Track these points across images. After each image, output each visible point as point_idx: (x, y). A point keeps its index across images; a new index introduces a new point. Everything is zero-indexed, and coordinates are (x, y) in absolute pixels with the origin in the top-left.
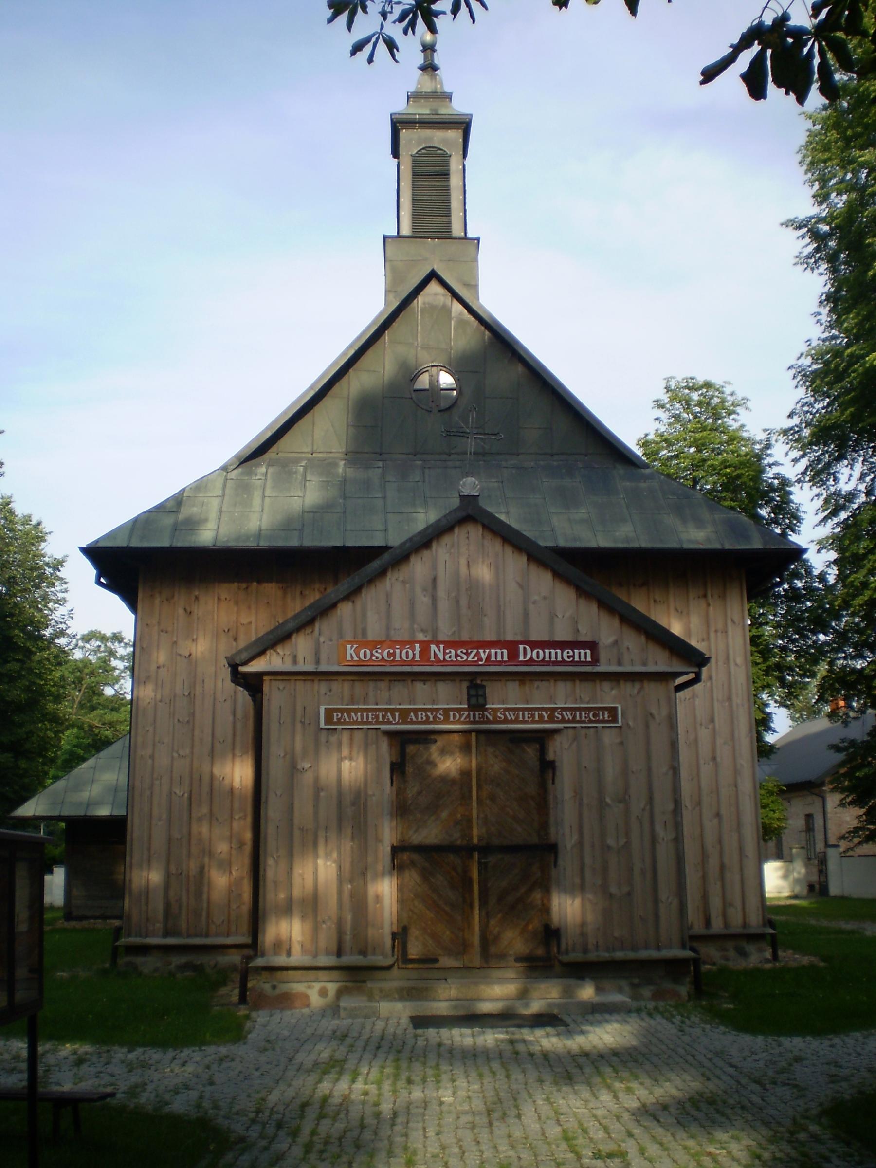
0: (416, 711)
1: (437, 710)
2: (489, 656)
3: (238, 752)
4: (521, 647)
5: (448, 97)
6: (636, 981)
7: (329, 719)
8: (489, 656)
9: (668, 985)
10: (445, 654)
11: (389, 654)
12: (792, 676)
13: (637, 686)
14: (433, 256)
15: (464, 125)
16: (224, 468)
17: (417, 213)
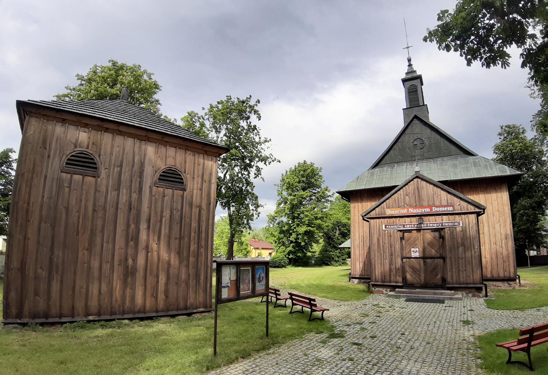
7: (386, 227)
9: (476, 293)
14: (416, 111)
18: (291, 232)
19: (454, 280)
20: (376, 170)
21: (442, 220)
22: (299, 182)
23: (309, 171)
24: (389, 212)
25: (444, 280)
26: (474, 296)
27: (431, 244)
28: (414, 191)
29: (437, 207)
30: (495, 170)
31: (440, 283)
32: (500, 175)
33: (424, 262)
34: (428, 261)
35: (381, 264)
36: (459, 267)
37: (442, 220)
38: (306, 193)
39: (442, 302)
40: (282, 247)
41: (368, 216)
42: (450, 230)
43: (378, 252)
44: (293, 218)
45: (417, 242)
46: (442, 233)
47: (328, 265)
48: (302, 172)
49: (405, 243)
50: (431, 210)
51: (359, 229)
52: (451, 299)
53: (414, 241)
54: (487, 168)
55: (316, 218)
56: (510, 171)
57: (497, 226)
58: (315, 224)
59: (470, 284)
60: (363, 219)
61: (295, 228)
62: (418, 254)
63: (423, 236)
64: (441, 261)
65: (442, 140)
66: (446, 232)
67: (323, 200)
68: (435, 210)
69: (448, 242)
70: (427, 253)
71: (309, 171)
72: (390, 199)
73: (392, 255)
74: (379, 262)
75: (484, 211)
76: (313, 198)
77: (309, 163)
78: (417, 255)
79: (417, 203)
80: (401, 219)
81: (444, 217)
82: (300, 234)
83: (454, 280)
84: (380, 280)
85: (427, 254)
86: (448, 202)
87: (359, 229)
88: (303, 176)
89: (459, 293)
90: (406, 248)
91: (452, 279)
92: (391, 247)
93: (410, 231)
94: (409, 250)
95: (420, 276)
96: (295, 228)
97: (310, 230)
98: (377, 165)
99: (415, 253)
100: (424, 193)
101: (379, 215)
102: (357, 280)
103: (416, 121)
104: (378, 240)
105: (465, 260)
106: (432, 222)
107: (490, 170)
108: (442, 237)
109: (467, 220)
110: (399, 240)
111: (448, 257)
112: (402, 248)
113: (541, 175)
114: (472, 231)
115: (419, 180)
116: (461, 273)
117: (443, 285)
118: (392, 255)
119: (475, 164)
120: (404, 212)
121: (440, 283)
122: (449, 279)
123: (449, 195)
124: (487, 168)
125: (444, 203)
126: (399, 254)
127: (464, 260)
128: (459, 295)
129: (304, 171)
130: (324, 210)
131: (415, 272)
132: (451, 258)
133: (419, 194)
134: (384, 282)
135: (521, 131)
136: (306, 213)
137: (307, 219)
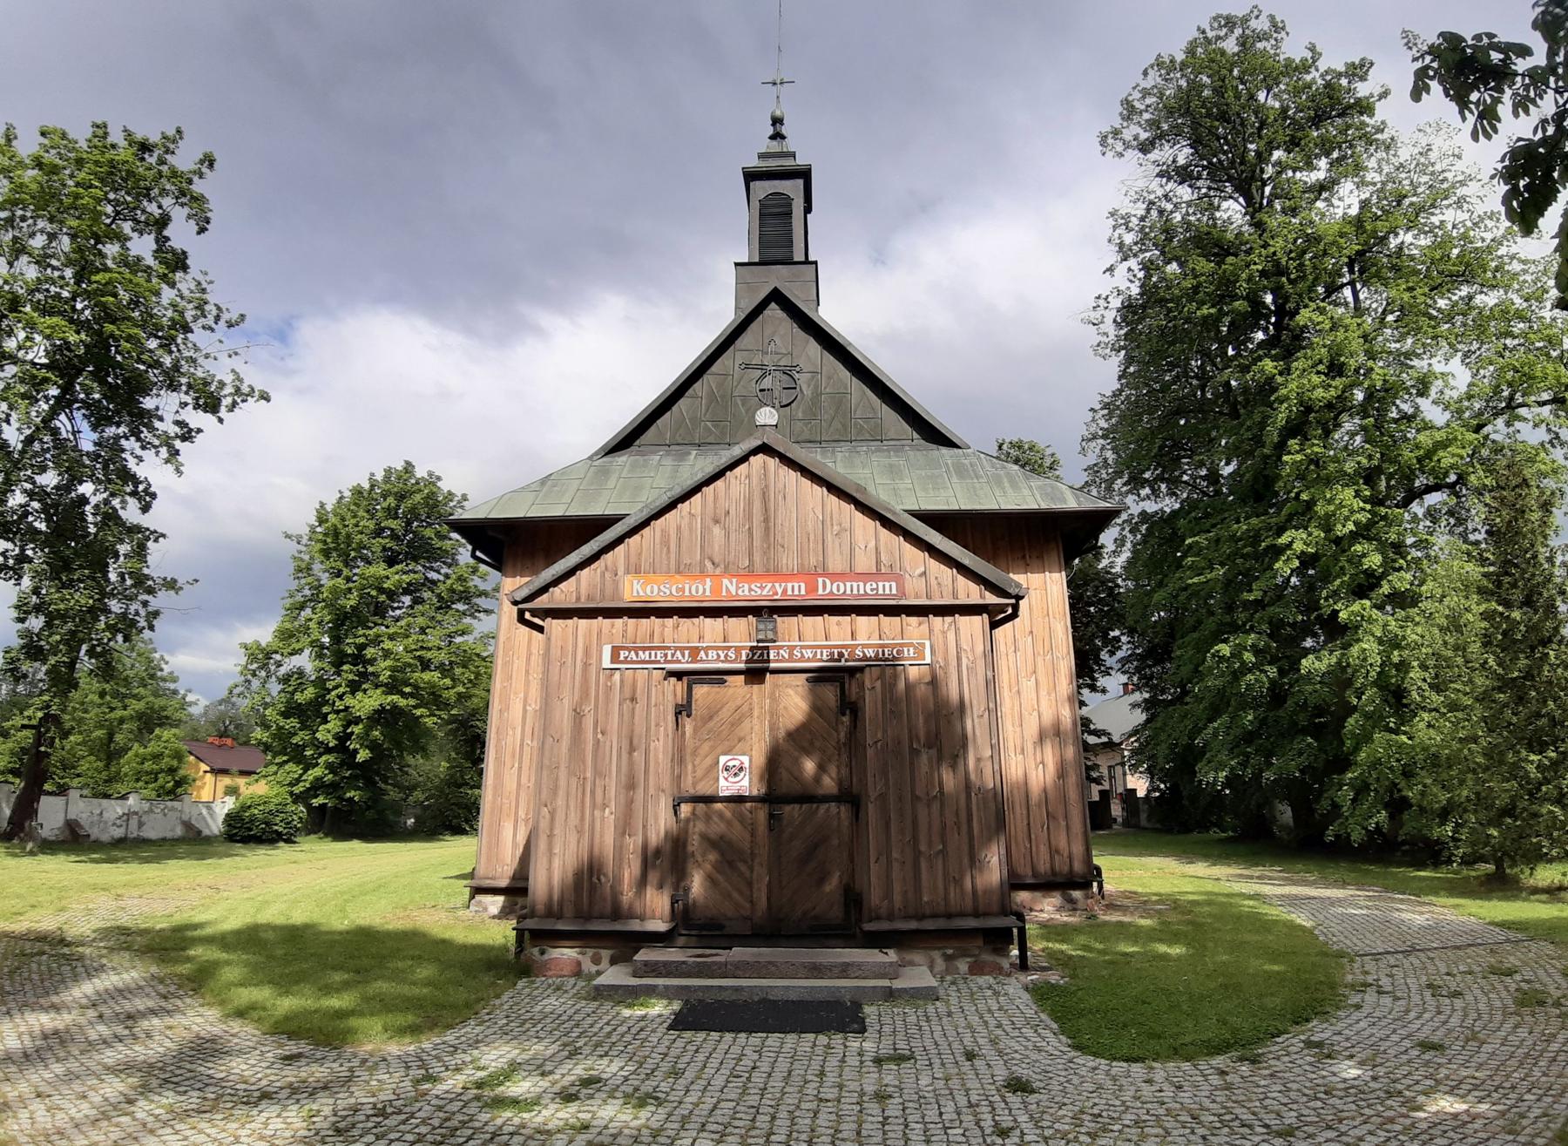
0: (706, 649)
1: (729, 648)
2: (785, 591)
3: (1018, 799)
4: (820, 580)
5: (793, 155)
6: (950, 952)
7: (615, 657)
8: (785, 591)
9: (987, 957)
10: (738, 588)
11: (678, 590)
12: (1261, 345)
13: (948, 619)
14: (777, 278)
15: (805, 174)
16: (590, 458)
17: (764, 243)
18: (325, 709)
19: (897, 899)
20: (622, 459)
21: (853, 636)
22: (378, 532)
23: (418, 498)
24: (635, 590)
25: (853, 899)
26: (977, 969)
27: (801, 738)
28: (750, 503)
29: (835, 577)
30: (1026, 492)
31: (836, 913)
32: (1044, 506)
33: (771, 816)
34: (791, 811)
35: (580, 832)
36: (915, 838)
37: (853, 636)
38: (395, 577)
39: (841, 1017)
40: (290, 766)
41: (542, 602)
42: (881, 677)
43: (571, 773)
44: (339, 660)
45: (746, 724)
46: (853, 690)
47: (462, 832)
48: (391, 501)
49: (695, 731)
50: (812, 588)
51: (527, 683)
52: (890, 995)
53: (736, 724)
54: (999, 483)
55: (426, 665)
56: (1077, 497)
57: (1028, 685)
58: (416, 687)
59: (962, 915)
60: (521, 619)
61: (340, 697)
62: (746, 782)
63: (774, 699)
64: (845, 811)
65: (856, 386)
66: (868, 684)
67: (460, 607)
68: (828, 590)
69: (872, 732)
70: (785, 775)
71: (418, 498)
72: (646, 531)
73: (631, 786)
74: (574, 819)
75: (1016, 608)
76: (426, 595)
77: (420, 472)
78: (744, 784)
79: (757, 558)
80: (686, 623)
81: (863, 621)
82: (357, 721)
83: (897, 899)
84: (569, 910)
85: (786, 785)
86: (878, 563)
87: (527, 683)
88: (392, 513)
89: (917, 957)
90: (695, 753)
91: (888, 894)
92: (632, 749)
93: (716, 677)
94: (709, 761)
95: (750, 884)
96: (340, 697)
97: (395, 706)
98: (625, 442)
99: (737, 775)
100: (786, 518)
101: (589, 598)
102: (500, 899)
103: (774, 310)
104: (578, 716)
105: (942, 805)
106: (808, 642)
107: (1010, 491)
108: (850, 707)
109: (951, 636)
110: (671, 717)
111: (873, 794)
112: (679, 756)
113: (1092, 580)
114: (964, 685)
115: (772, 463)
116: (924, 865)
117: (851, 925)
118: (631, 786)
119: (961, 471)
120: (699, 591)
121: (836, 913)
122: (875, 897)
123: (884, 533)
124: (999, 483)
125: (864, 563)
126: (666, 783)
127: (936, 806)
128: (919, 975)
129: (401, 497)
130: (458, 640)
131: (731, 864)
132: (883, 797)
133: (766, 520)
134: (589, 917)
135: (1048, 462)
136: (387, 645)
137: (388, 663)
